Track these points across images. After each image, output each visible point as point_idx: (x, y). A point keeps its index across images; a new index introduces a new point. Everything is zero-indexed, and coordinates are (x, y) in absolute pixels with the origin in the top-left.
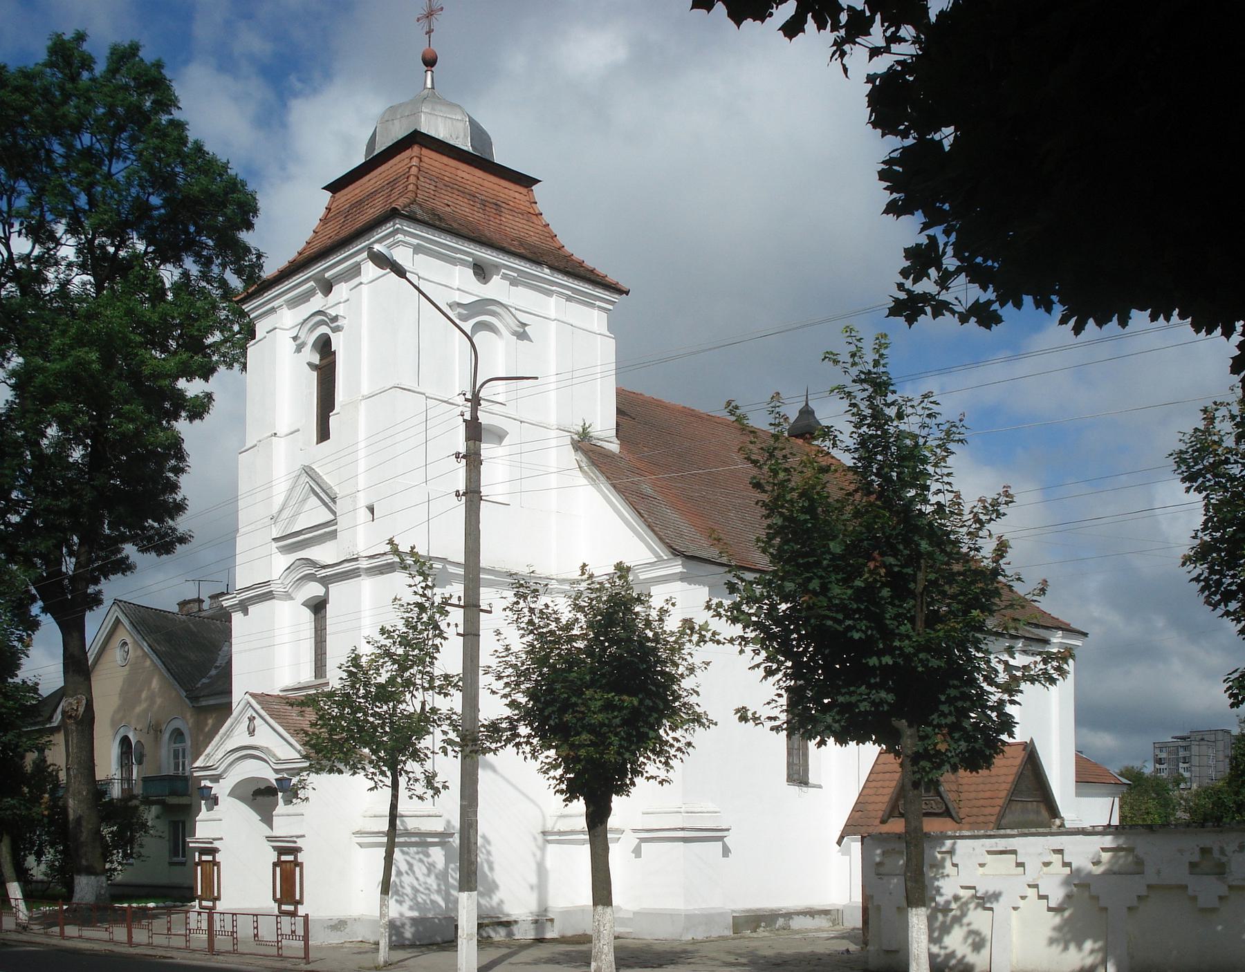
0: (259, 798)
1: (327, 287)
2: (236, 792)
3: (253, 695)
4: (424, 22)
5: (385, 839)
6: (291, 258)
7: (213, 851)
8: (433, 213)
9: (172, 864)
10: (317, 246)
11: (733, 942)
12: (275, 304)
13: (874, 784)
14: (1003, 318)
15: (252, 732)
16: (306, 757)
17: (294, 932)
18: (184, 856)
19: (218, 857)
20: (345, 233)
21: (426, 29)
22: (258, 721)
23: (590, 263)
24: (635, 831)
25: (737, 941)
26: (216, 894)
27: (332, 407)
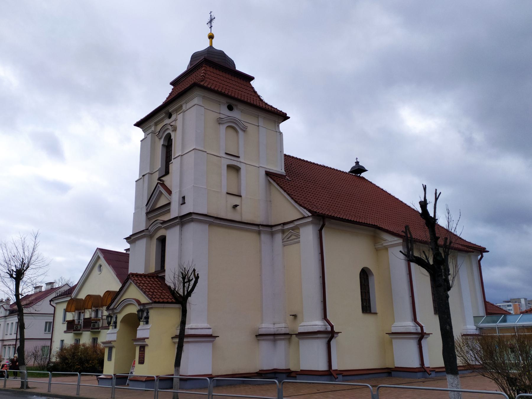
1: (170, 116)
21: (210, 26)
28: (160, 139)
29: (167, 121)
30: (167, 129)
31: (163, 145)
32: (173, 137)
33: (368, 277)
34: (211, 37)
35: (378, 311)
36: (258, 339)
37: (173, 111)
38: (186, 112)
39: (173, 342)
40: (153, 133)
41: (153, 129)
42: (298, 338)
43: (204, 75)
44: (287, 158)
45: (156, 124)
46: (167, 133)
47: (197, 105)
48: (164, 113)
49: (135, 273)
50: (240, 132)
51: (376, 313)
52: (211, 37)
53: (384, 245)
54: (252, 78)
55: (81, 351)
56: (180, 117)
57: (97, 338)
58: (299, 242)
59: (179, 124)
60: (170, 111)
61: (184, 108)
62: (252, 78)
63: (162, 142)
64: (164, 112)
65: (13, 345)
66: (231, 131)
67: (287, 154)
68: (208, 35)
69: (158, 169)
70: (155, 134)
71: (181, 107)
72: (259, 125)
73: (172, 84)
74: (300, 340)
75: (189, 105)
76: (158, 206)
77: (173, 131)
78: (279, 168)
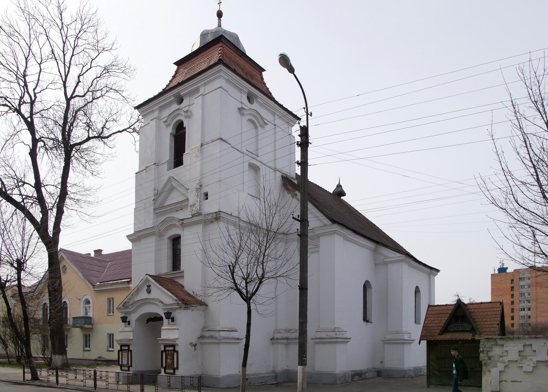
1: (180, 100)
2: (138, 320)
12: (154, 109)
13: (428, 319)
15: (149, 292)
19: (131, 348)
22: (152, 288)
28: (168, 126)
30: (179, 115)
34: (220, 15)
36: (272, 343)
37: (186, 95)
38: (205, 96)
39: (200, 342)
40: (158, 118)
41: (156, 114)
42: (120, 312)
43: (222, 55)
45: (161, 108)
46: (177, 120)
47: (24, 144)
48: (173, 96)
50: (259, 128)
51: (372, 323)
52: (220, 15)
53: (385, 261)
54: (264, 70)
57: (89, 335)
58: (318, 251)
60: (181, 94)
61: (202, 91)
62: (264, 70)
64: (174, 95)
65: (197, 387)
66: (251, 126)
69: (166, 161)
70: (160, 120)
71: (197, 90)
73: (176, 63)
74: (316, 344)
75: (209, 88)
76: (167, 203)
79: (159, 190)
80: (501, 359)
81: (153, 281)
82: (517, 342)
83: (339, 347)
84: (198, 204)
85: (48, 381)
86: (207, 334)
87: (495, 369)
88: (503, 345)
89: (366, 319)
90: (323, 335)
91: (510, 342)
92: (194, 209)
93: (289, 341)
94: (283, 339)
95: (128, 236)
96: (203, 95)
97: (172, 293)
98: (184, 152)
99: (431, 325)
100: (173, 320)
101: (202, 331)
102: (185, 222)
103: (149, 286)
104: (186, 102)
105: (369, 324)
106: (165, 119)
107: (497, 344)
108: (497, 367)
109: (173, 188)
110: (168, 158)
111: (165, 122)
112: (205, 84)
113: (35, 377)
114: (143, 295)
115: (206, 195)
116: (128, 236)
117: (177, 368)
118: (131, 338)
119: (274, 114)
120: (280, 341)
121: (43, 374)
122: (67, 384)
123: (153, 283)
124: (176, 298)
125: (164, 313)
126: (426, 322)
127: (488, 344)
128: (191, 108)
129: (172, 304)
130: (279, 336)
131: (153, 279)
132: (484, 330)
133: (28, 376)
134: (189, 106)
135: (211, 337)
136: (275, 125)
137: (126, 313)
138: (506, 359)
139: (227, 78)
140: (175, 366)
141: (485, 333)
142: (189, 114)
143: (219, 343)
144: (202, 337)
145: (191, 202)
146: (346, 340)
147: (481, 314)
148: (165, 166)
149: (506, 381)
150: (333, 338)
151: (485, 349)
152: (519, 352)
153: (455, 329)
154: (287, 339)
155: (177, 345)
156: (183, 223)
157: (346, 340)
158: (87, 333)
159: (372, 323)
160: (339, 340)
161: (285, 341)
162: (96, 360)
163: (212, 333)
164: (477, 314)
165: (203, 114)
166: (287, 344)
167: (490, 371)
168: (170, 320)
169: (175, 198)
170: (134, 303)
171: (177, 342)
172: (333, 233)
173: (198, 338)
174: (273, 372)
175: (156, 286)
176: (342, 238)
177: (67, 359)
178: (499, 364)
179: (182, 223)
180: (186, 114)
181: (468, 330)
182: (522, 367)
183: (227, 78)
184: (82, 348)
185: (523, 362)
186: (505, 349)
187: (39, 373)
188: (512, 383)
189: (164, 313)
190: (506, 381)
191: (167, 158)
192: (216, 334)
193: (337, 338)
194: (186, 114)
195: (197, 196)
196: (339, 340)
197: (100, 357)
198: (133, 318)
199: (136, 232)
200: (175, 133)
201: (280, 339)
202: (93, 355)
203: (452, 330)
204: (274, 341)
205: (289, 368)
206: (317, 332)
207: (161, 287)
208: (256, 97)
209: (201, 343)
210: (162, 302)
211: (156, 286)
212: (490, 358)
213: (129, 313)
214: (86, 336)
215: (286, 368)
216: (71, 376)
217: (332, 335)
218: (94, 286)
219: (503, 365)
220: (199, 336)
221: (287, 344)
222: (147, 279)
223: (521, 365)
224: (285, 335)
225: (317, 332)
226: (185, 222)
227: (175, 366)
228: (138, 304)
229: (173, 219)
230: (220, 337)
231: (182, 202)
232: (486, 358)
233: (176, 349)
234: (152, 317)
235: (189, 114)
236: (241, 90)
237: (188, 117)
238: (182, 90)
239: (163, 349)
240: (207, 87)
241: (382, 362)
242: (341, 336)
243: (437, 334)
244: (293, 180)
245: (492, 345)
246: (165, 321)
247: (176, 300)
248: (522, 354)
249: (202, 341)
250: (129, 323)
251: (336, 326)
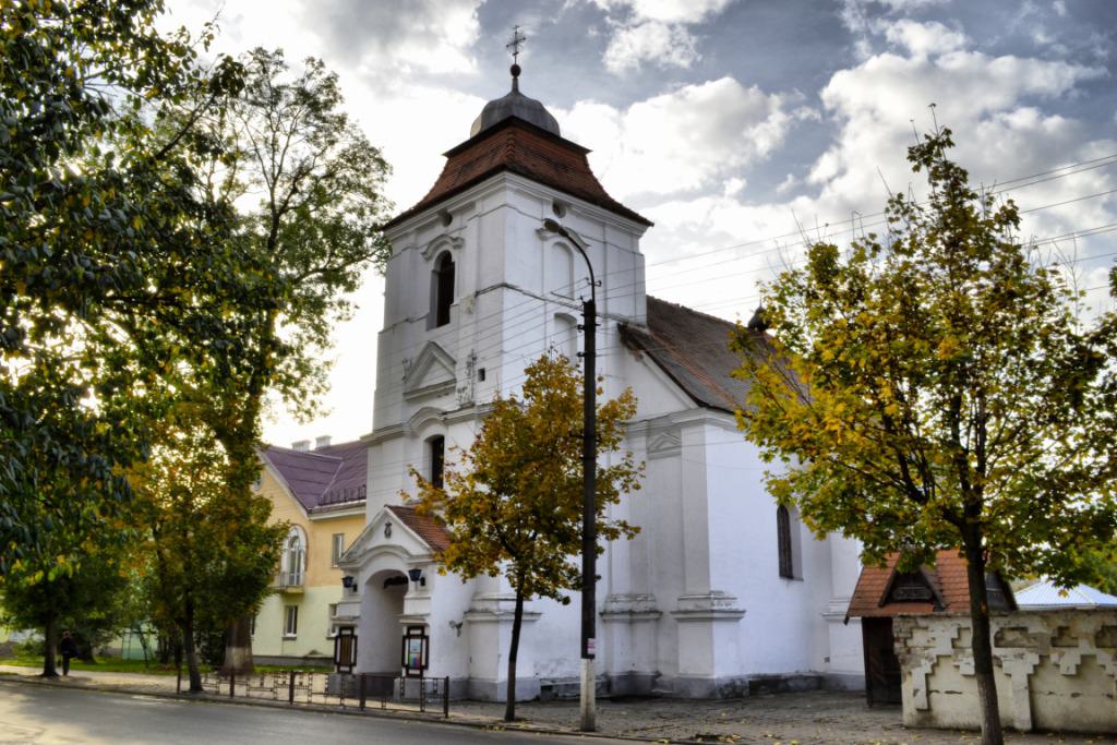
0: (390, 587)
1: (448, 219)
2: (372, 581)
3: (391, 507)
4: (512, 47)
5: (513, 618)
6: (419, 201)
7: (351, 628)
8: (528, 170)
9: (285, 639)
10: (438, 194)
11: (543, 735)
12: (409, 231)
13: (866, 577)
14: (572, 113)
15: (388, 534)
16: (431, 556)
17: (435, 691)
18: (295, 632)
19: (356, 632)
20: (458, 184)
21: (513, 52)
22: (393, 528)
23: (626, 205)
24: (673, 613)
25: (547, 735)
26: (352, 660)
27: (451, 300)
28: (428, 259)
29: (440, 229)
31: (434, 271)
32: (454, 258)
33: (787, 514)
35: (804, 575)
37: (454, 212)
44: (653, 304)
45: (421, 230)
49: (358, 439)
51: (802, 580)
55: (251, 475)
56: (472, 226)
57: (296, 608)
58: (679, 454)
59: (470, 237)
62: (588, 151)
63: (431, 265)
67: (657, 296)
68: (627, 113)
70: (417, 248)
71: (472, 206)
72: (608, 239)
76: (423, 385)
77: (455, 247)
78: (639, 314)
79: (414, 361)
80: (926, 652)
81: (395, 516)
82: (947, 623)
83: (720, 631)
84: (469, 387)
85: (217, 693)
86: (480, 606)
87: (918, 669)
88: (926, 628)
89: (787, 571)
90: (690, 606)
91: (937, 623)
92: (463, 395)
93: (635, 617)
94: (623, 613)
95: (428, 330)
96: (480, 216)
97: (423, 537)
98: (452, 301)
99: (868, 588)
100: (423, 582)
101: (473, 600)
102: (449, 416)
103: (389, 525)
104: (456, 222)
105: (795, 585)
106: (424, 250)
107: (918, 628)
108: (920, 666)
109: (434, 359)
110: (427, 311)
111: (424, 254)
112: (484, 198)
113: (196, 687)
114: (380, 539)
115: (482, 373)
116: (428, 330)
117: (426, 667)
118: (357, 614)
119: (604, 225)
120: (616, 617)
121: (210, 683)
122: (248, 696)
123: (396, 522)
124: (428, 546)
125: (410, 572)
126: (861, 583)
127: (906, 627)
128: (463, 234)
129: (422, 556)
130: (614, 607)
131: (396, 513)
132: (954, 599)
133: (186, 685)
134: (461, 229)
135: (486, 611)
136: (605, 243)
137: (353, 570)
138: (934, 653)
139: (515, 187)
140: (423, 663)
141: (954, 605)
142: (459, 242)
143: (497, 622)
144: (471, 611)
145: (459, 385)
146: (735, 616)
147: (954, 568)
148: (424, 323)
149: (937, 692)
150: (707, 611)
151: (901, 635)
152: (953, 640)
153: (905, 597)
154: (631, 612)
155: (427, 625)
156: (447, 419)
157: (735, 616)
158: (293, 604)
159: (802, 580)
160: (716, 615)
161: (627, 617)
162: (305, 658)
163: (487, 605)
164: (947, 568)
165: (479, 244)
166: (631, 622)
167: (910, 673)
168: (419, 582)
169: (437, 376)
170: (366, 552)
171: (428, 620)
172: (702, 422)
173: (465, 613)
174: (605, 675)
175: (399, 525)
176: (722, 430)
177: (251, 656)
178: (923, 661)
179: (446, 419)
180: (456, 243)
181: (926, 598)
182: (957, 667)
183: (515, 187)
184: (282, 635)
185: (960, 657)
186: (931, 635)
187: (203, 680)
188: (946, 695)
189: (410, 572)
190: (937, 692)
191: (427, 310)
192: (492, 606)
193: (713, 611)
194: (456, 243)
195: (469, 374)
196: (716, 615)
197: (314, 652)
198: (362, 579)
199: (376, 431)
200: (439, 270)
201: (617, 614)
202: (299, 649)
203: (900, 598)
204: (606, 617)
205: (634, 669)
206: (680, 599)
207: (407, 528)
208: (569, 205)
209: (470, 622)
210: (407, 553)
211: (399, 525)
212: (909, 651)
213: (356, 571)
214: (291, 611)
215: (629, 668)
216: (255, 683)
217: (706, 605)
218: (310, 512)
219: (929, 665)
220: (467, 609)
221: (631, 622)
222: (386, 514)
223: (956, 664)
224: (627, 607)
225: (680, 599)
226: (449, 416)
227: (423, 663)
228: (371, 555)
229: (431, 410)
230: (499, 610)
231: (446, 383)
232: (903, 650)
233: (426, 634)
234: (393, 576)
235: (459, 242)
236: (541, 201)
237: (458, 247)
238: (450, 205)
239: (405, 633)
240: (487, 201)
241: (827, 660)
242: (724, 607)
243: (876, 606)
244: (641, 329)
245: (911, 629)
246: (411, 584)
247: (428, 549)
248: (958, 644)
249: (470, 618)
250: (355, 588)
251: (712, 589)
